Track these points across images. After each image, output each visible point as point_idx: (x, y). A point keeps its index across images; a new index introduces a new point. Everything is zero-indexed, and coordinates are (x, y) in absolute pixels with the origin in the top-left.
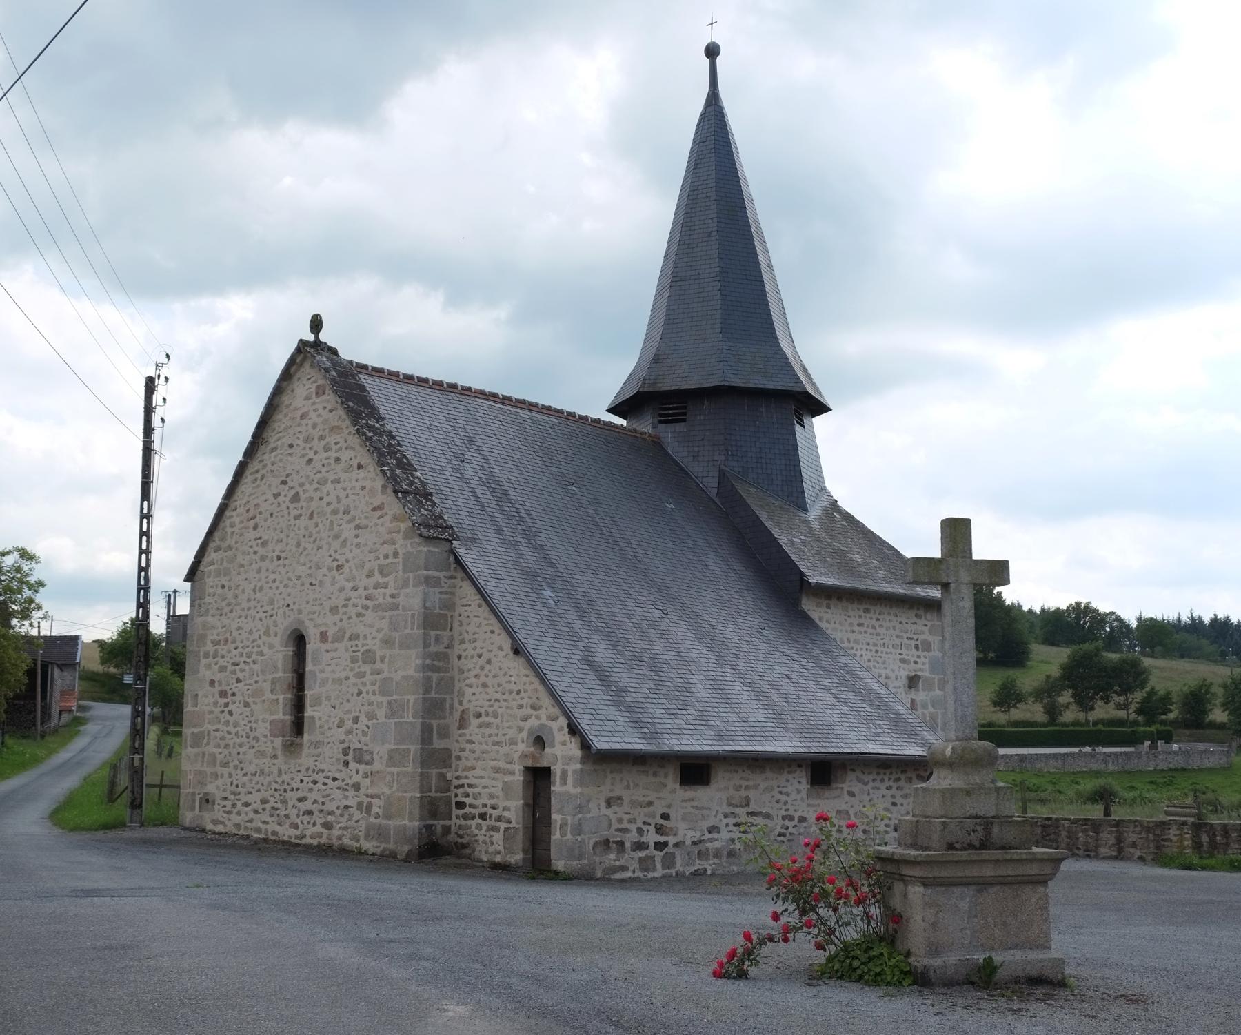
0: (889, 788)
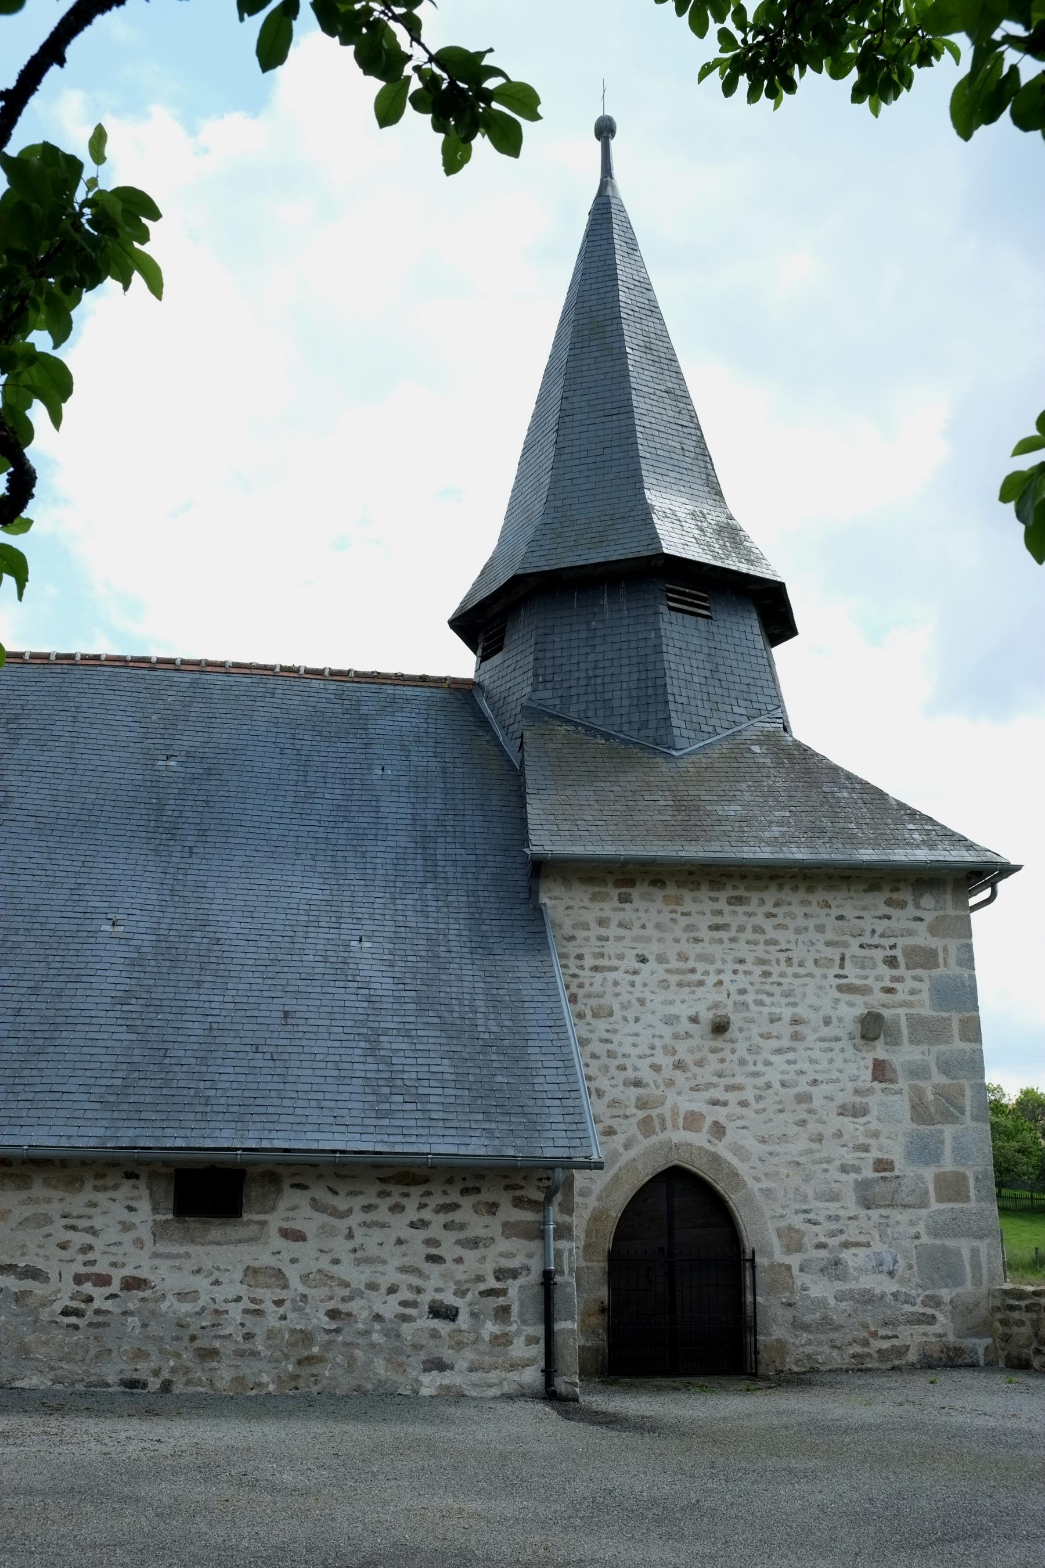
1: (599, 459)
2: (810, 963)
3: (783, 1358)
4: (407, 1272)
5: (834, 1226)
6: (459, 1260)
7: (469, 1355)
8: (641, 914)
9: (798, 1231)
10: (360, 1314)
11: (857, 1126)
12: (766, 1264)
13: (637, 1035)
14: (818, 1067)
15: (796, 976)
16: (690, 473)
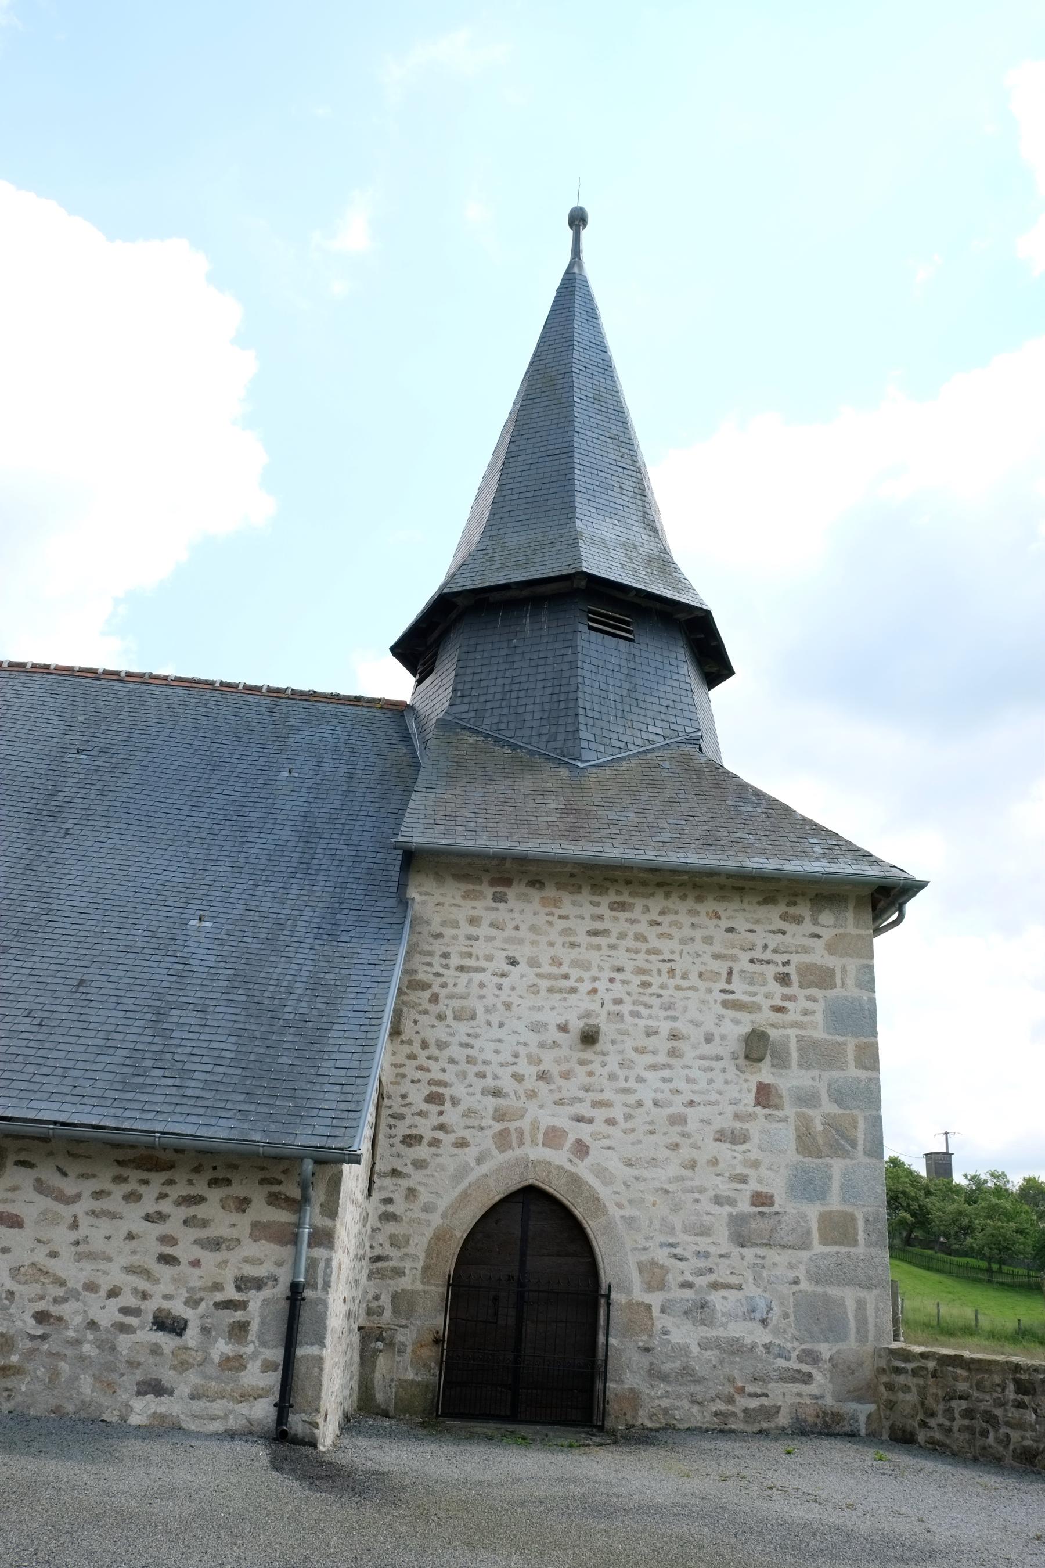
0: (155, 1218)
1: (536, 493)
2: (694, 976)
3: (635, 1410)
4: (134, 1272)
5: (702, 1264)
6: (196, 1263)
7: (193, 1378)
8: (516, 915)
9: (662, 1267)
10: (72, 1319)
11: (735, 1154)
12: (623, 1302)
13: (500, 1041)
14: (696, 1087)
15: (678, 988)
16: (626, 509)
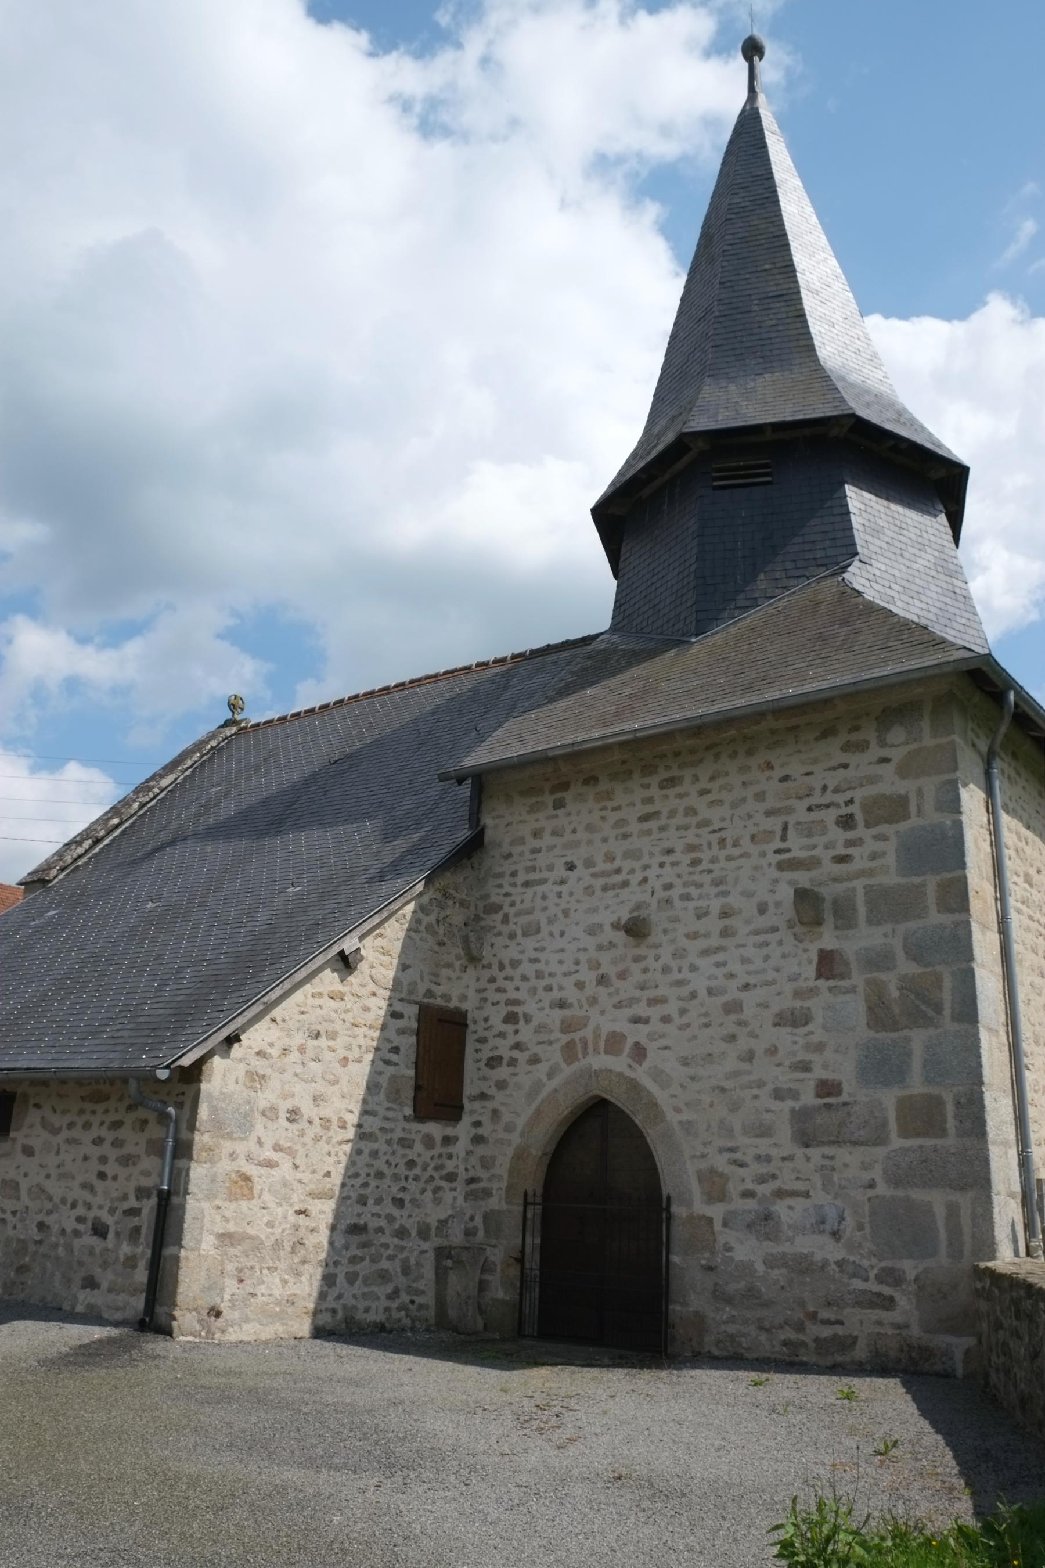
0: (98, 1141)
